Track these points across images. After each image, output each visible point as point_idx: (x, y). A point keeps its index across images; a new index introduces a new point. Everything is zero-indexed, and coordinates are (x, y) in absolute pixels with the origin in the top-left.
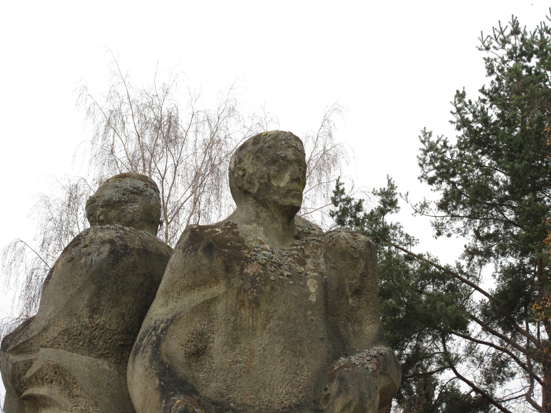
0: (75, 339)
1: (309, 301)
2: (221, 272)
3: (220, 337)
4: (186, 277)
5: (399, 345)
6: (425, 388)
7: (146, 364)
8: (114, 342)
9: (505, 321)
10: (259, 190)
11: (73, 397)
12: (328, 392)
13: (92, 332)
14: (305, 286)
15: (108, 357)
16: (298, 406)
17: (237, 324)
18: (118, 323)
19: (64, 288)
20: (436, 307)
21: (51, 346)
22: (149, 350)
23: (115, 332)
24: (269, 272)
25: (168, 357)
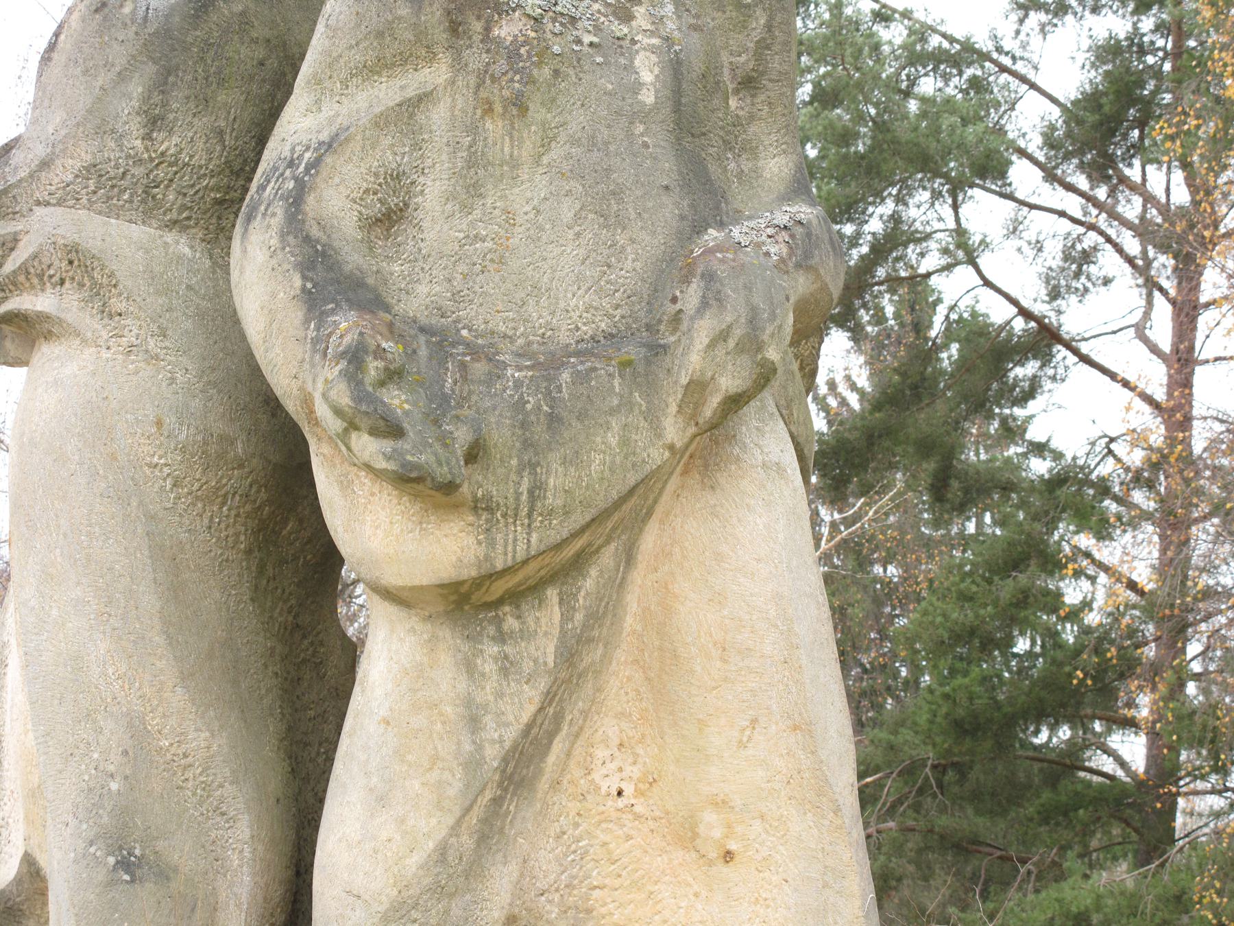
0: (113, 187)
1: (639, 102)
2: (440, 35)
3: (438, 183)
5: (855, 212)
6: (913, 309)
7: (273, 242)
8: (201, 194)
9: (1094, 161)
11: (111, 316)
12: (678, 306)
13: (151, 171)
14: (630, 68)
15: (188, 227)
16: (612, 336)
17: (476, 152)
19: (86, 72)
20: (940, 127)
21: (60, 203)
22: (280, 212)
23: (202, 172)
24: (549, 36)
25: (323, 228)
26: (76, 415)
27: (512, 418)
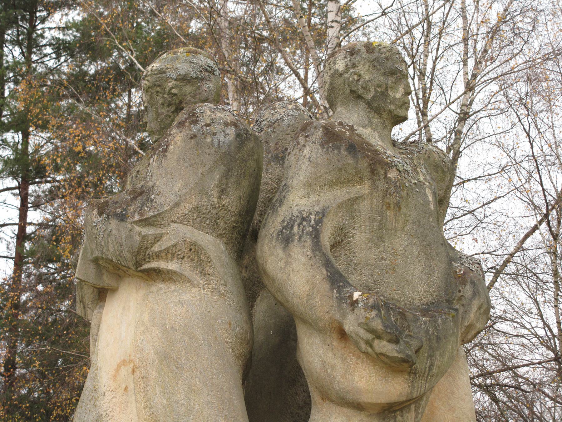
0: (204, 217)
2: (367, 173)
3: (363, 234)
4: (331, 173)
10: (374, 97)
11: (205, 275)
16: (433, 303)
17: (382, 224)
18: (237, 206)
19: (192, 165)
26: (198, 318)
27: (426, 337)
